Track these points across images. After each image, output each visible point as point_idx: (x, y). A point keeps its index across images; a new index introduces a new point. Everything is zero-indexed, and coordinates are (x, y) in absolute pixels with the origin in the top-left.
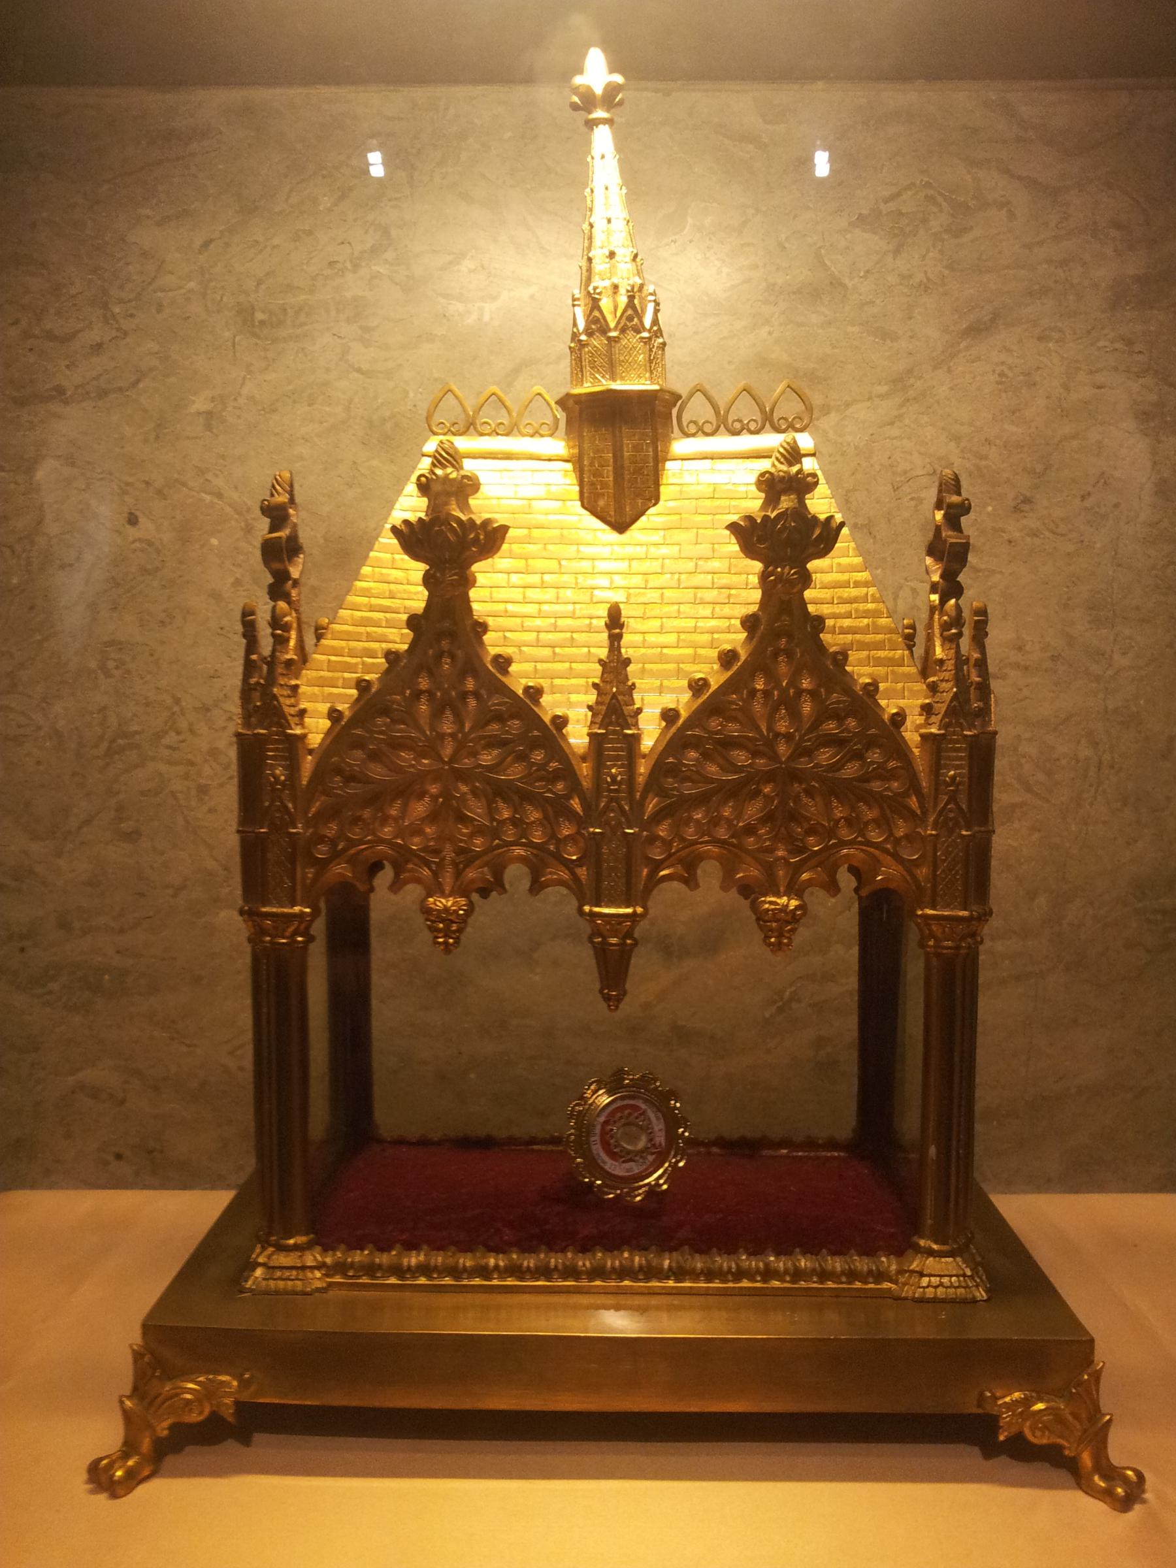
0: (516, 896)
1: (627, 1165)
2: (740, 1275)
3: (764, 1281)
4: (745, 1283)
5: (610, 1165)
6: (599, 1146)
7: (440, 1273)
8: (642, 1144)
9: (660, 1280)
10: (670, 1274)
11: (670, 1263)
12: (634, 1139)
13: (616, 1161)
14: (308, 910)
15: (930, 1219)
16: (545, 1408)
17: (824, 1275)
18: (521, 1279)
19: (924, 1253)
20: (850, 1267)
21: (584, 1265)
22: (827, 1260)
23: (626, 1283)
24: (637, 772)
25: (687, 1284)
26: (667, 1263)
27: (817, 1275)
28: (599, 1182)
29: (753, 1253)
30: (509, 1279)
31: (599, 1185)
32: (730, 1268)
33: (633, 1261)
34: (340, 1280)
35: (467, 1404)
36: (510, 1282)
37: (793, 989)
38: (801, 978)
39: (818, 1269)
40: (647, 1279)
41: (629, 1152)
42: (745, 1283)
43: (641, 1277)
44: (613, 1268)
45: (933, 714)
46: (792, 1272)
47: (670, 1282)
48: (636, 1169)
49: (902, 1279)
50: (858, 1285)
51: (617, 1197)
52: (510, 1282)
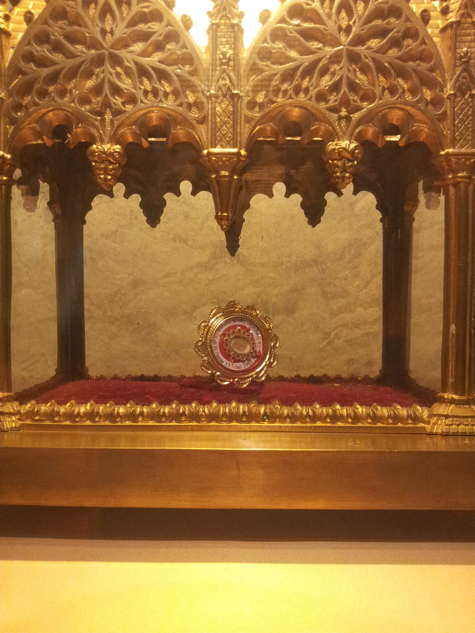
0: (184, 281)
1: (237, 364)
2: (314, 418)
3: (332, 422)
4: (319, 424)
5: (226, 363)
6: (218, 350)
7: (100, 417)
8: (248, 349)
9: (258, 422)
10: (265, 417)
11: (265, 409)
12: (243, 347)
13: (230, 360)
14: (9, 156)
15: (452, 378)
16: (169, 506)
17: (375, 418)
18: (160, 421)
19: (447, 403)
20: (395, 413)
21: (204, 411)
22: (377, 409)
23: (234, 424)
24: (241, 57)
25: (277, 424)
26: (262, 410)
27: (371, 418)
28: (218, 373)
29: (323, 404)
30: (151, 422)
31: (218, 375)
32: (308, 413)
33: (238, 409)
34: (30, 423)
35: (111, 503)
36: (151, 423)
37: (335, 332)
38: (340, 326)
39: (372, 414)
40: (250, 422)
41: (238, 355)
42: (319, 424)
43: (244, 419)
44: (225, 413)
45: (450, 12)
46: (352, 416)
47: (266, 423)
48: (242, 366)
49: (433, 420)
50: (400, 425)
51: (231, 384)
52: (151, 423)
